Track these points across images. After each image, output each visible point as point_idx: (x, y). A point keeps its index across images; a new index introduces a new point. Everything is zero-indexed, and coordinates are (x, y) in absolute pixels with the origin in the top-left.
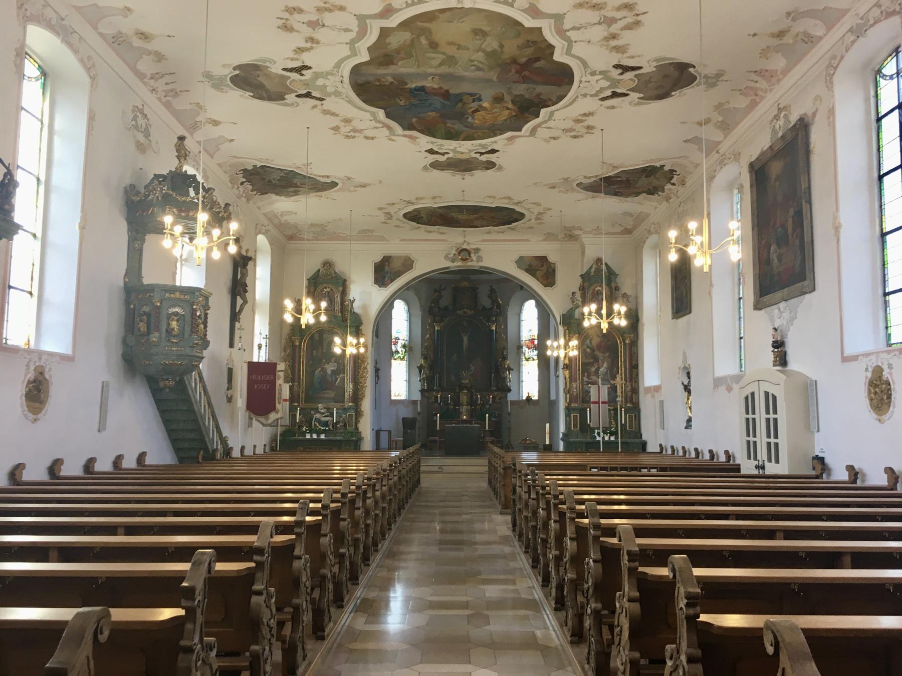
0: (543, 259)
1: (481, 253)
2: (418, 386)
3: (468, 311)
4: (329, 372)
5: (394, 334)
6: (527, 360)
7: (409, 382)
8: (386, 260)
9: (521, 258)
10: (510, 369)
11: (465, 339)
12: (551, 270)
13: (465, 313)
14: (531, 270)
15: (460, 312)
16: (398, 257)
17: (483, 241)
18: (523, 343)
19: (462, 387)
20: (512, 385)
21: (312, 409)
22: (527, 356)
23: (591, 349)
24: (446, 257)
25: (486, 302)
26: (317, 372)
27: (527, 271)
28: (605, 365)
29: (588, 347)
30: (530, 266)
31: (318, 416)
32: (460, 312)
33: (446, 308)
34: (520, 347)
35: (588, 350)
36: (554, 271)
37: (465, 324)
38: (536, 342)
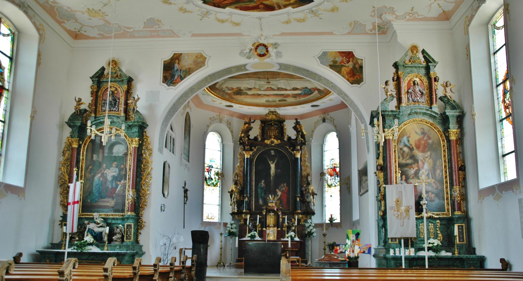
0: (349, 55)
1: (279, 49)
2: (229, 208)
3: (275, 141)
4: (109, 178)
5: (207, 162)
6: (330, 186)
7: (222, 206)
8: (177, 57)
9: (325, 54)
10: (313, 194)
11: (273, 166)
12: (357, 66)
13: (272, 142)
14: (335, 67)
15: (268, 142)
16: (188, 54)
17: (283, 34)
18: (325, 171)
19: (269, 211)
20: (316, 208)
21: (87, 219)
22: (329, 183)
23: (409, 147)
24: (241, 53)
25: (290, 132)
26: (96, 178)
27: (331, 67)
28: (426, 166)
29: (406, 146)
30: (335, 62)
31: (92, 226)
32: (268, 142)
33: (256, 138)
34: (322, 174)
35: (406, 149)
36: (361, 67)
37: (273, 152)
38: (338, 170)
